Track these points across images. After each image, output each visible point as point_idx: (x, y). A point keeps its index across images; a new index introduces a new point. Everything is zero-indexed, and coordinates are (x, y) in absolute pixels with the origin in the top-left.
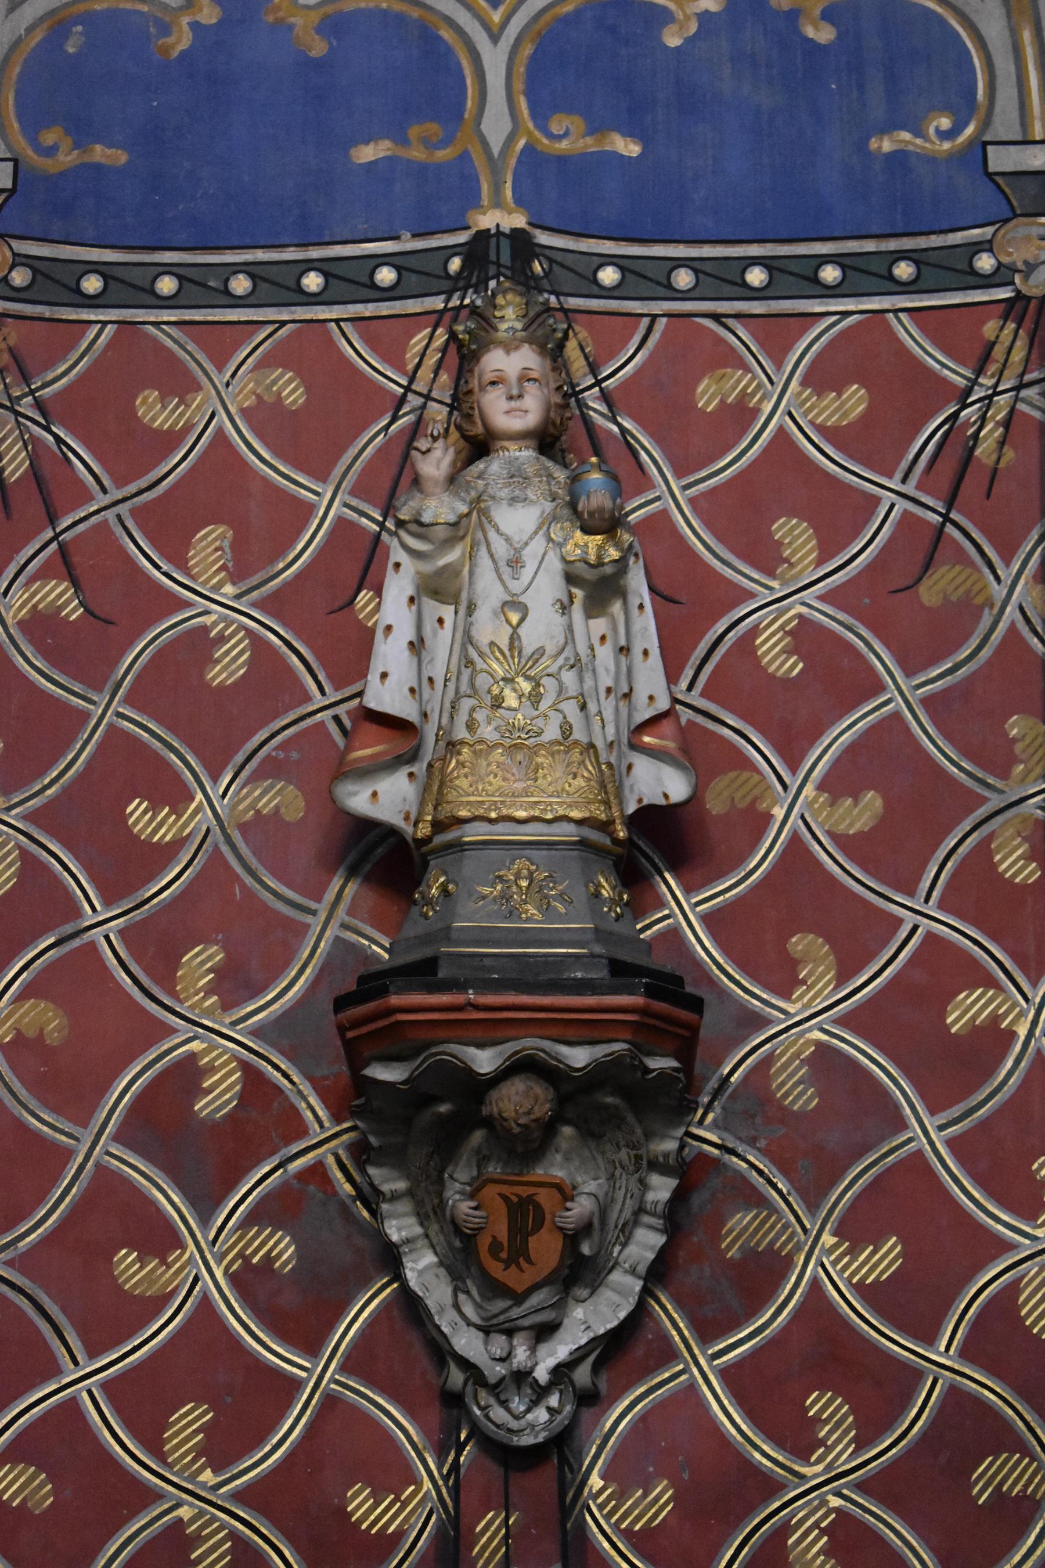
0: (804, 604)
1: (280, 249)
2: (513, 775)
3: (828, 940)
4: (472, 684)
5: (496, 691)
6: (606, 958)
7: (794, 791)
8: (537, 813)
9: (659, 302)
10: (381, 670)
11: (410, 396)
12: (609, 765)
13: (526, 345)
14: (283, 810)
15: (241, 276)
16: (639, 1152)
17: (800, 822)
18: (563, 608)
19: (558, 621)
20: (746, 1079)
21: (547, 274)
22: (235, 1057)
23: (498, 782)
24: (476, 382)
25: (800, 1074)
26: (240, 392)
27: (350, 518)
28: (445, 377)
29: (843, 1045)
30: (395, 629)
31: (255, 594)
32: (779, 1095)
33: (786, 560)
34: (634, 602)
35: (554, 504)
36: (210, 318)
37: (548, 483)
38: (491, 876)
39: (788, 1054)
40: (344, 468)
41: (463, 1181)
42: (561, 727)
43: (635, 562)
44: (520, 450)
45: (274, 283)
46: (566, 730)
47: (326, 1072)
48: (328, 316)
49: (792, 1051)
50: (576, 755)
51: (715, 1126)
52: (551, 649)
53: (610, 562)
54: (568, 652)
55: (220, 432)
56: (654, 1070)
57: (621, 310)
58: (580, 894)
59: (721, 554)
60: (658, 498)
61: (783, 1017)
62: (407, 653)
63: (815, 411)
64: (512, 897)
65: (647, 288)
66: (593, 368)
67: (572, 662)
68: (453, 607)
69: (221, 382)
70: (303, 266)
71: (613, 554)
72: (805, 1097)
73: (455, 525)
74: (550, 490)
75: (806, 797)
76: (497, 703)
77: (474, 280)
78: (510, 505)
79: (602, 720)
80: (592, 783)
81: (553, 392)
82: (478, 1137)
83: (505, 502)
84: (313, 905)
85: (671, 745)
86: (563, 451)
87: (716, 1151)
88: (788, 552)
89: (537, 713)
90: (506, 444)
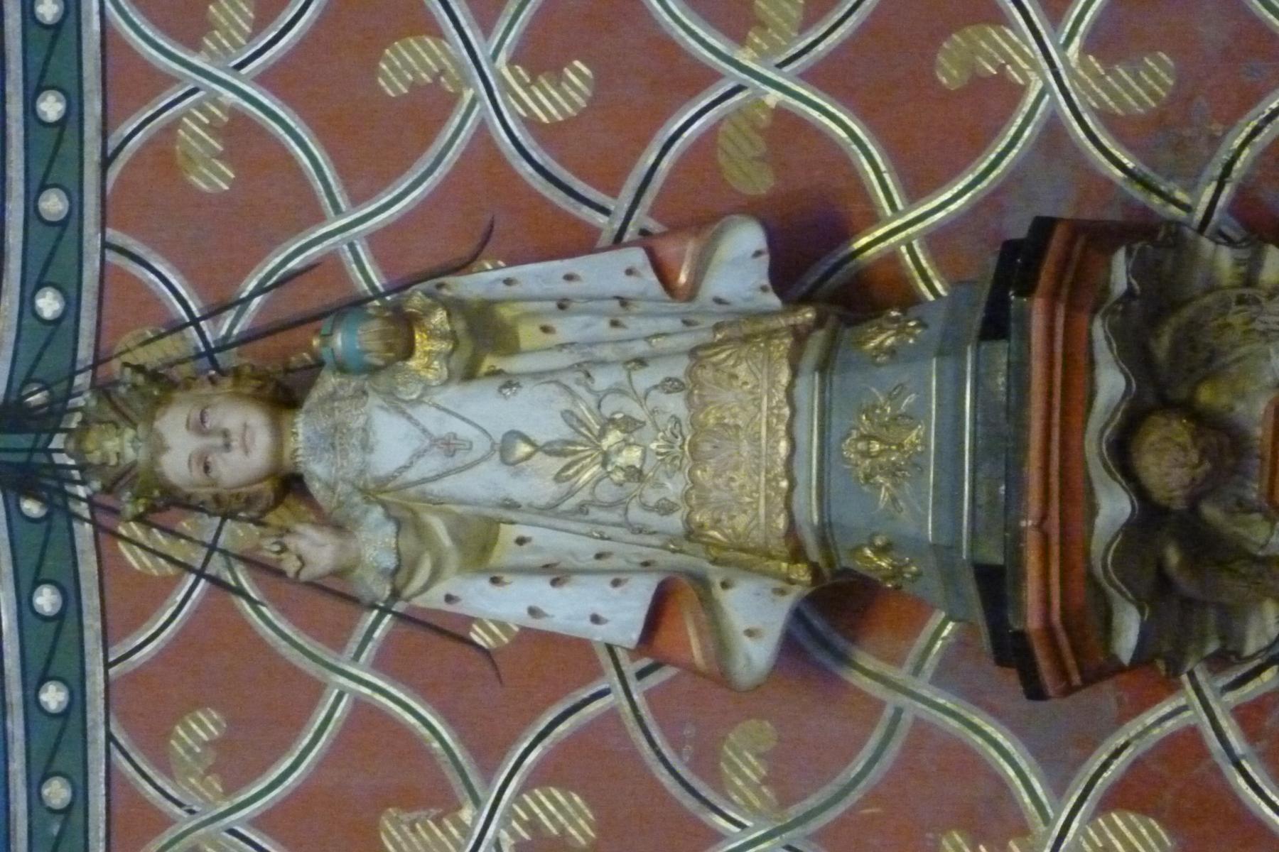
0: (495, 56)
1: (10, 740)
2: (730, 456)
3: (945, 33)
4: (610, 506)
5: (619, 476)
6: (978, 346)
7: (745, 76)
8: (782, 427)
9: (86, 238)
10: (587, 623)
11: (210, 571)
12: (717, 328)
13: (157, 424)
14: (762, 749)
15: (46, 792)
16: (1234, 299)
17: (786, 69)
18: (509, 385)
19: (529, 393)
20: (1130, 148)
21: (46, 386)
22: (1091, 819)
23: (740, 478)
24: (203, 490)
25: (1125, 76)
26: (203, 796)
27: (373, 653)
28: (184, 524)
29: (1088, 18)
30: (532, 604)
31: (475, 780)
32: (1153, 105)
33: (436, 78)
34: (501, 290)
35: (371, 392)
36: (102, 834)
37: (343, 399)
38: (866, 489)
39: (1099, 90)
40: (307, 660)
41: (1268, 532)
42: (668, 392)
43: (448, 288)
44: (296, 434)
45: (56, 748)
46: (670, 385)
47: (1113, 700)
48: (100, 678)
49: (1094, 86)
50: (707, 374)
51: (1191, 189)
52: (564, 403)
53: (450, 322)
54: (569, 379)
55: (255, 823)
56: (1129, 284)
57: (96, 289)
58: (890, 374)
59: (427, 165)
60: (352, 246)
61: (1047, 97)
62: (567, 590)
63: (235, 33)
64: (894, 463)
65: (66, 255)
66: (176, 327)
67: (581, 375)
68: (502, 526)
69: (189, 821)
70: (33, 708)
71: (439, 317)
72: (1157, 70)
73: (399, 524)
74: (352, 397)
75: (753, 60)
76: (636, 474)
77: (53, 483)
78: (372, 450)
79: (657, 336)
80: (743, 354)
81: (218, 390)
82: (1211, 512)
83: (368, 457)
84: (888, 712)
85: (691, 247)
86: (288, 370)
87: (1227, 190)
88: (424, 75)
89: (649, 423)
90: (287, 453)
